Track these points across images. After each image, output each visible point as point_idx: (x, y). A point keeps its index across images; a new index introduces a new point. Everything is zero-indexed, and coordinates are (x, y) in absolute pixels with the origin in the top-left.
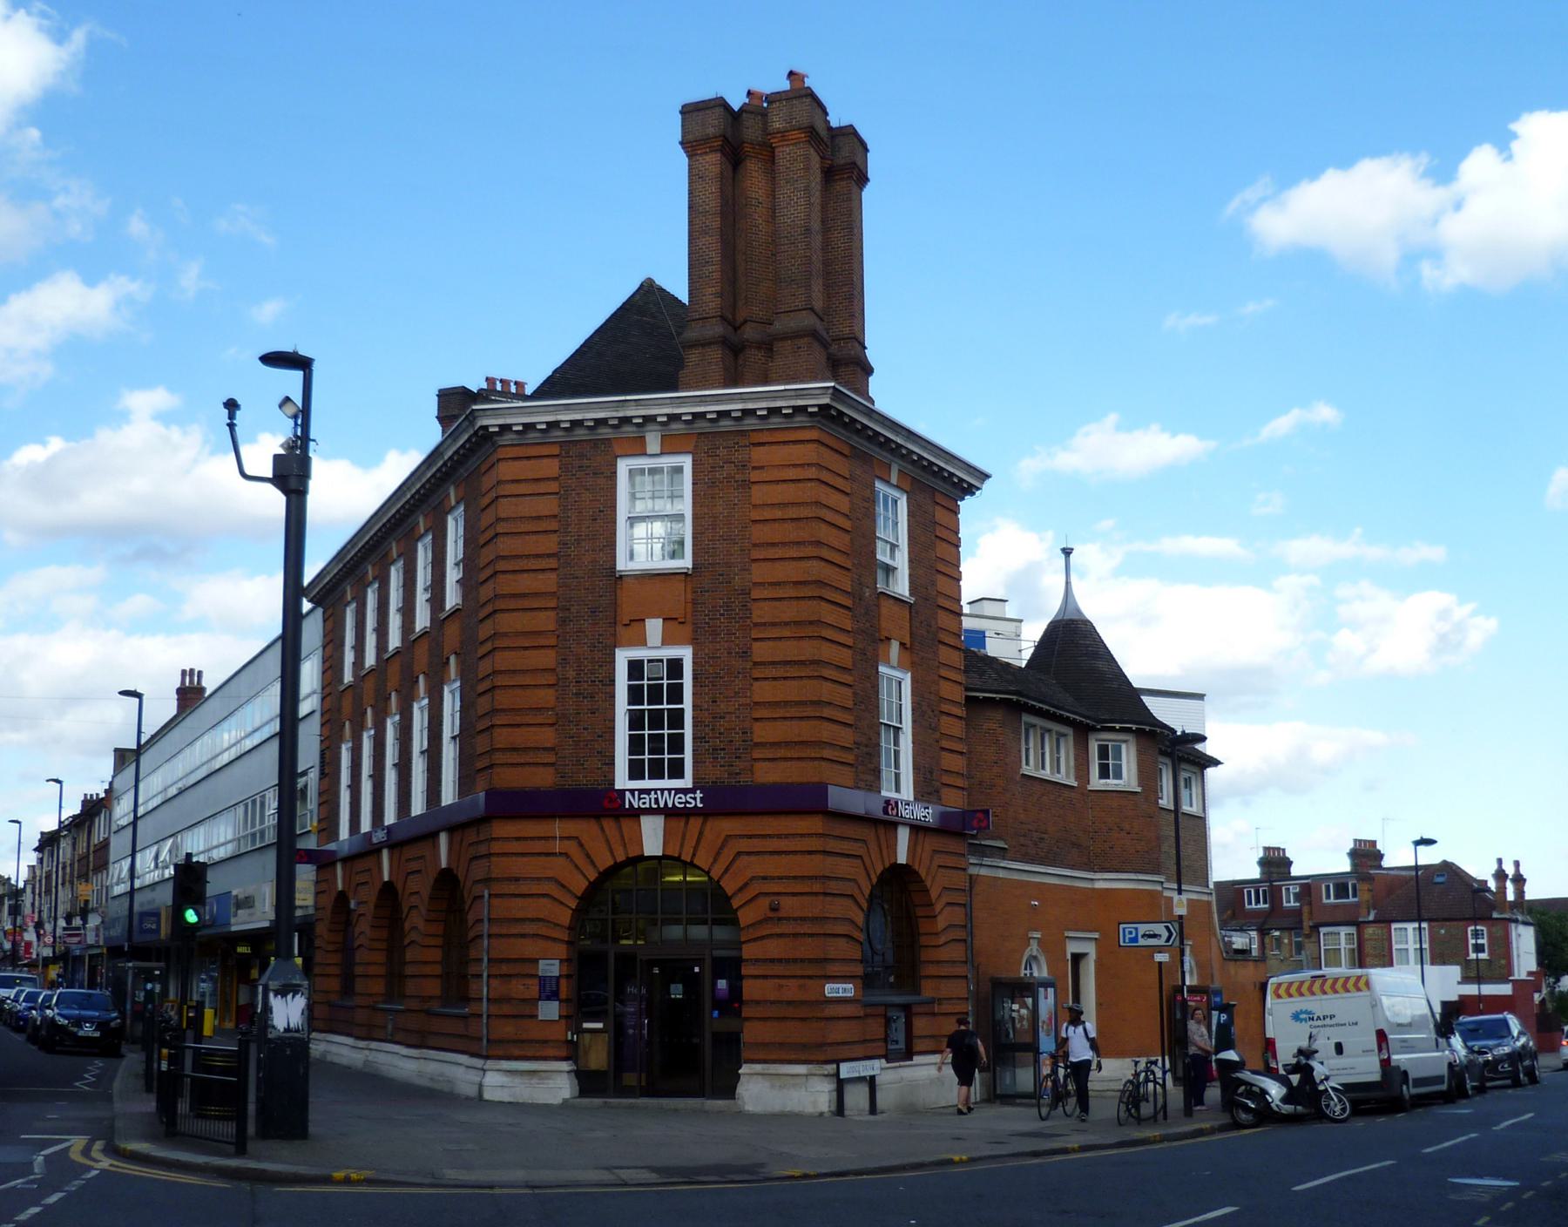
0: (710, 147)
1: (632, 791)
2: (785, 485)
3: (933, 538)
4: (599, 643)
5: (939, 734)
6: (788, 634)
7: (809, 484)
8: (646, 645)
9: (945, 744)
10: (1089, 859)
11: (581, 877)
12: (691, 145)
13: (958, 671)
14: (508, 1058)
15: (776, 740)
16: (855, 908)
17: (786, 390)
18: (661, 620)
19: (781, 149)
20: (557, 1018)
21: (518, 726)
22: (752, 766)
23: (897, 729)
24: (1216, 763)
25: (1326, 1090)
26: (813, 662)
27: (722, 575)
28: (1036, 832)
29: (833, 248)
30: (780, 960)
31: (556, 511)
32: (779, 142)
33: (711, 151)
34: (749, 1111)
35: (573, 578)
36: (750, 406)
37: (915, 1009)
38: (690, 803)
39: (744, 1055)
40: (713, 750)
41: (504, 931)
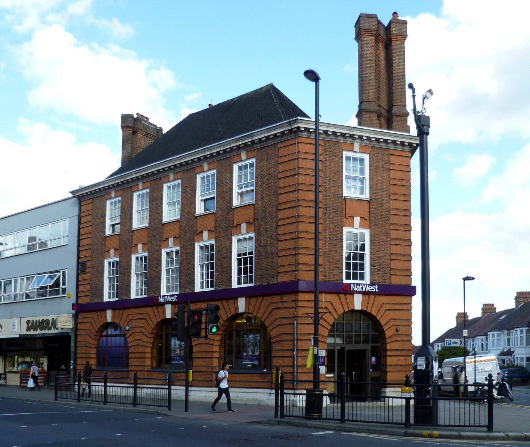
0: (372, 33)
1: (354, 284)
4: (338, 224)
19: (395, 42)
27: (380, 203)
30: (398, 350)
33: (371, 35)
36: (395, 139)
38: (373, 290)
40: (377, 270)
41: (304, 338)
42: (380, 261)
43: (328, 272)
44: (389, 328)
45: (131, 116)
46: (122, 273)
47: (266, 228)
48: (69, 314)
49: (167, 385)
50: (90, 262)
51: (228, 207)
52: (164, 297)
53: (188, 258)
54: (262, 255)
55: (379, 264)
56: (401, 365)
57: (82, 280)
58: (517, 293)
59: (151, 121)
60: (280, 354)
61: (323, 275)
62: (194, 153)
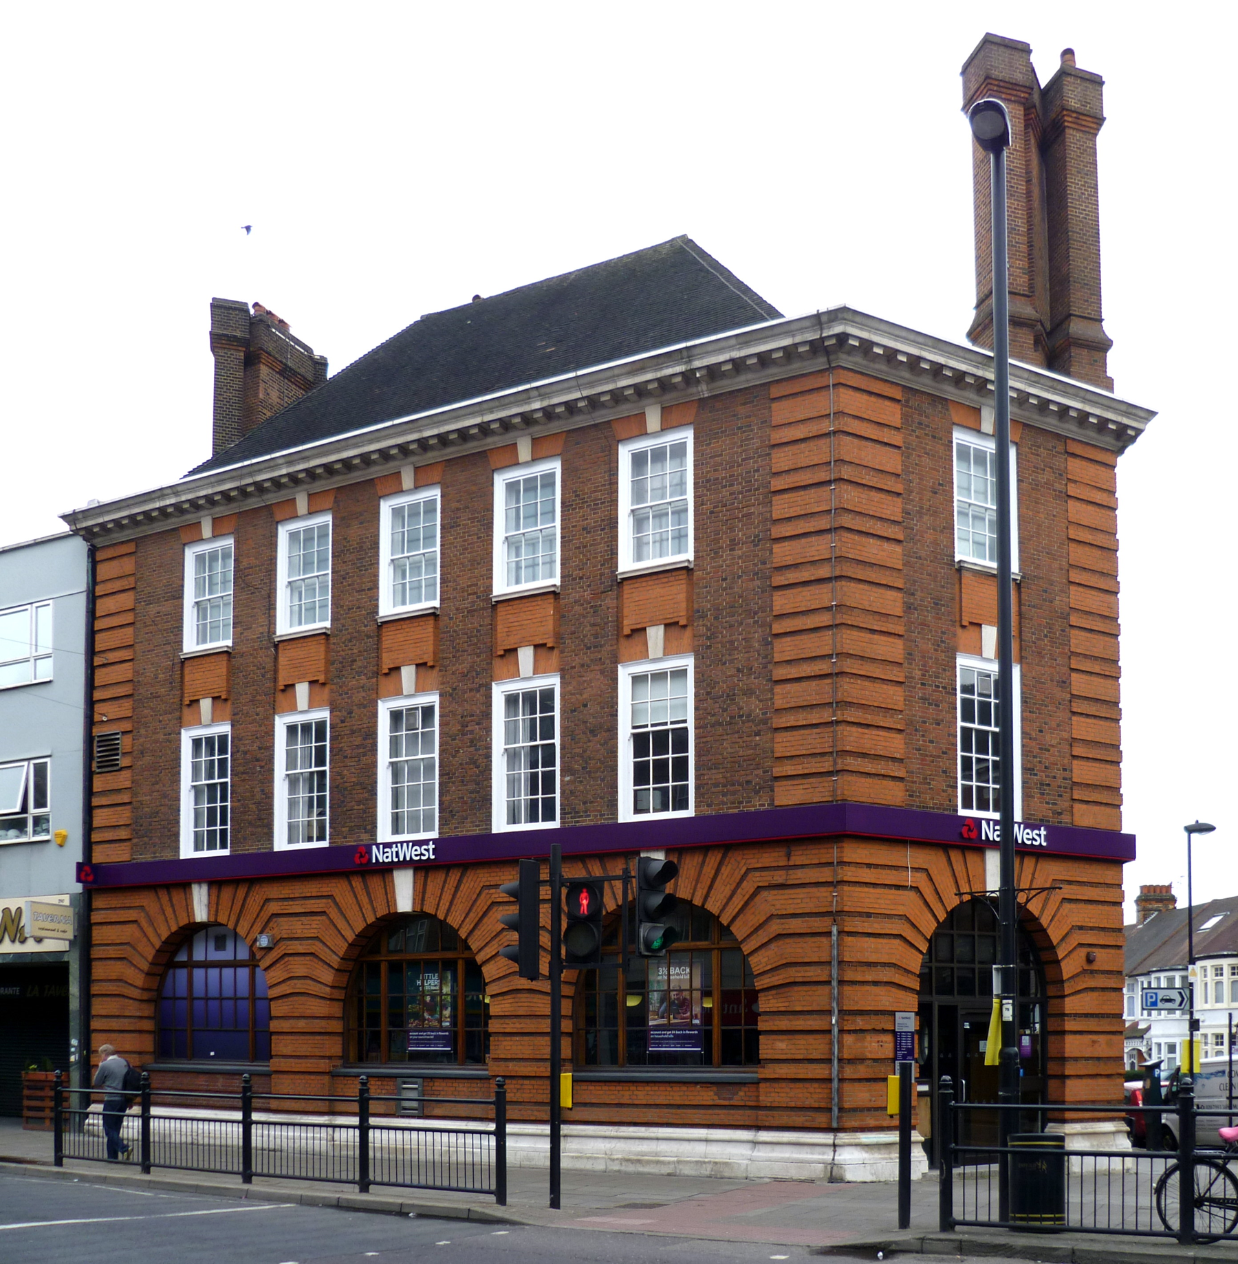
1: (988, 821)
4: (942, 642)
11: (930, 916)
14: (863, 1129)
18: (662, 627)
19: (1071, 131)
21: (868, 726)
22: (1072, 807)
27: (1046, 592)
33: (1015, 101)
43: (920, 783)
44: (1070, 952)
45: (240, 308)
46: (243, 773)
47: (732, 642)
48: (61, 897)
49: (490, 1120)
50: (130, 736)
51: (602, 575)
52: (391, 848)
53: (469, 728)
54: (720, 724)
55: (1046, 767)
56: (1099, 1059)
57: (102, 793)
58: (1142, 888)
59: (293, 331)
60: (784, 1024)
61: (907, 791)
62: (491, 404)
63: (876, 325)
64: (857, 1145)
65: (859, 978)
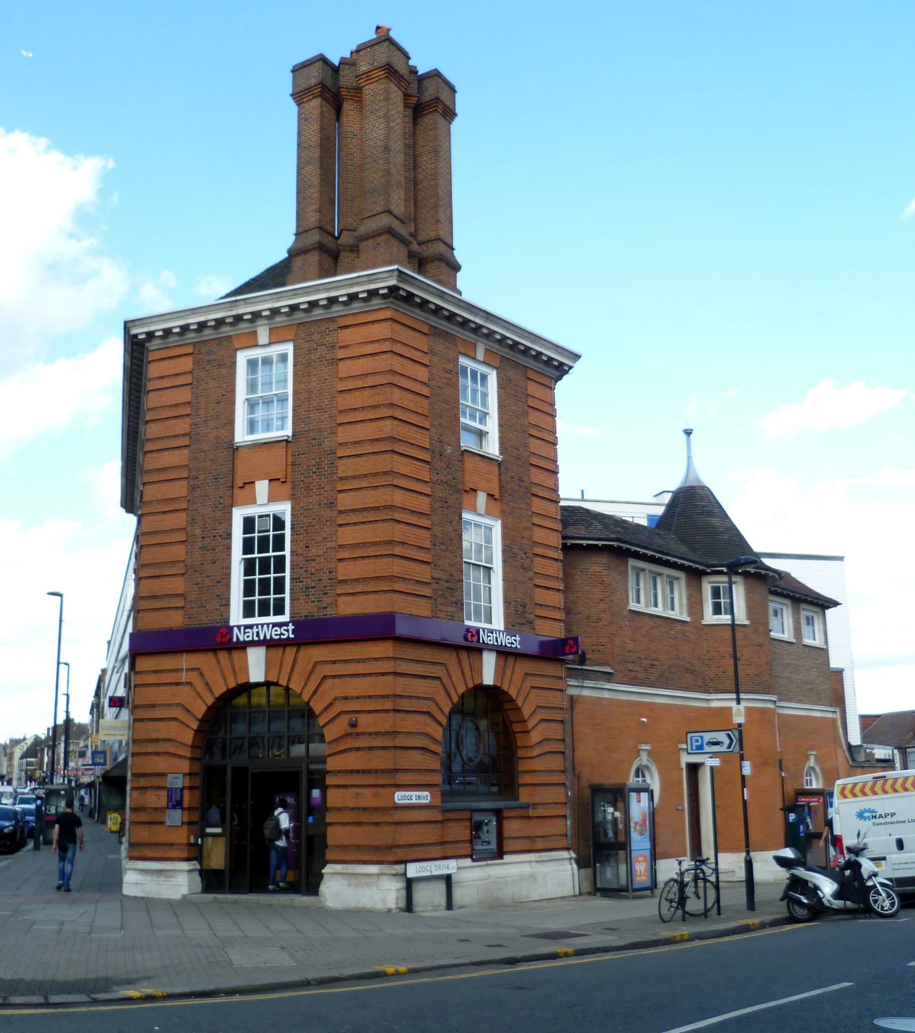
0: (313, 94)
2: (365, 359)
3: (526, 407)
4: (219, 504)
5: (532, 573)
6: (365, 484)
7: (384, 356)
8: (256, 503)
9: (538, 581)
10: (705, 682)
11: (201, 702)
12: (299, 96)
13: (554, 520)
15: (357, 577)
16: (434, 725)
17: (359, 277)
20: (180, 824)
23: (488, 570)
24: (836, 604)
25: (874, 886)
26: (386, 507)
27: (315, 439)
28: (646, 659)
29: (423, 169)
30: (358, 771)
31: (189, 398)
32: (365, 81)
33: (313, 98)
34: (329, 907)
35: (201, 452)
36: (333, 294)
37: (506, 814)
38: (284, 635)
39: (329, 855)
40: (306, 588)
42: (313, 567)
55: (311, 574)
56: (365, 809)
63: (150, 320)
64: (135, 869)
65: (143, 751)
